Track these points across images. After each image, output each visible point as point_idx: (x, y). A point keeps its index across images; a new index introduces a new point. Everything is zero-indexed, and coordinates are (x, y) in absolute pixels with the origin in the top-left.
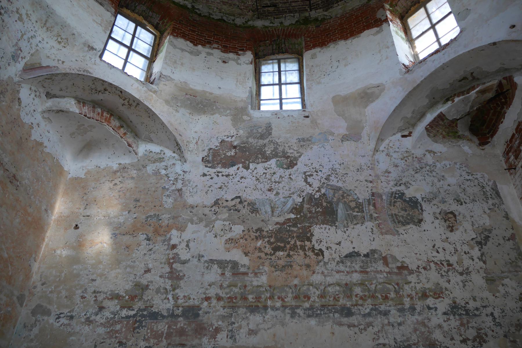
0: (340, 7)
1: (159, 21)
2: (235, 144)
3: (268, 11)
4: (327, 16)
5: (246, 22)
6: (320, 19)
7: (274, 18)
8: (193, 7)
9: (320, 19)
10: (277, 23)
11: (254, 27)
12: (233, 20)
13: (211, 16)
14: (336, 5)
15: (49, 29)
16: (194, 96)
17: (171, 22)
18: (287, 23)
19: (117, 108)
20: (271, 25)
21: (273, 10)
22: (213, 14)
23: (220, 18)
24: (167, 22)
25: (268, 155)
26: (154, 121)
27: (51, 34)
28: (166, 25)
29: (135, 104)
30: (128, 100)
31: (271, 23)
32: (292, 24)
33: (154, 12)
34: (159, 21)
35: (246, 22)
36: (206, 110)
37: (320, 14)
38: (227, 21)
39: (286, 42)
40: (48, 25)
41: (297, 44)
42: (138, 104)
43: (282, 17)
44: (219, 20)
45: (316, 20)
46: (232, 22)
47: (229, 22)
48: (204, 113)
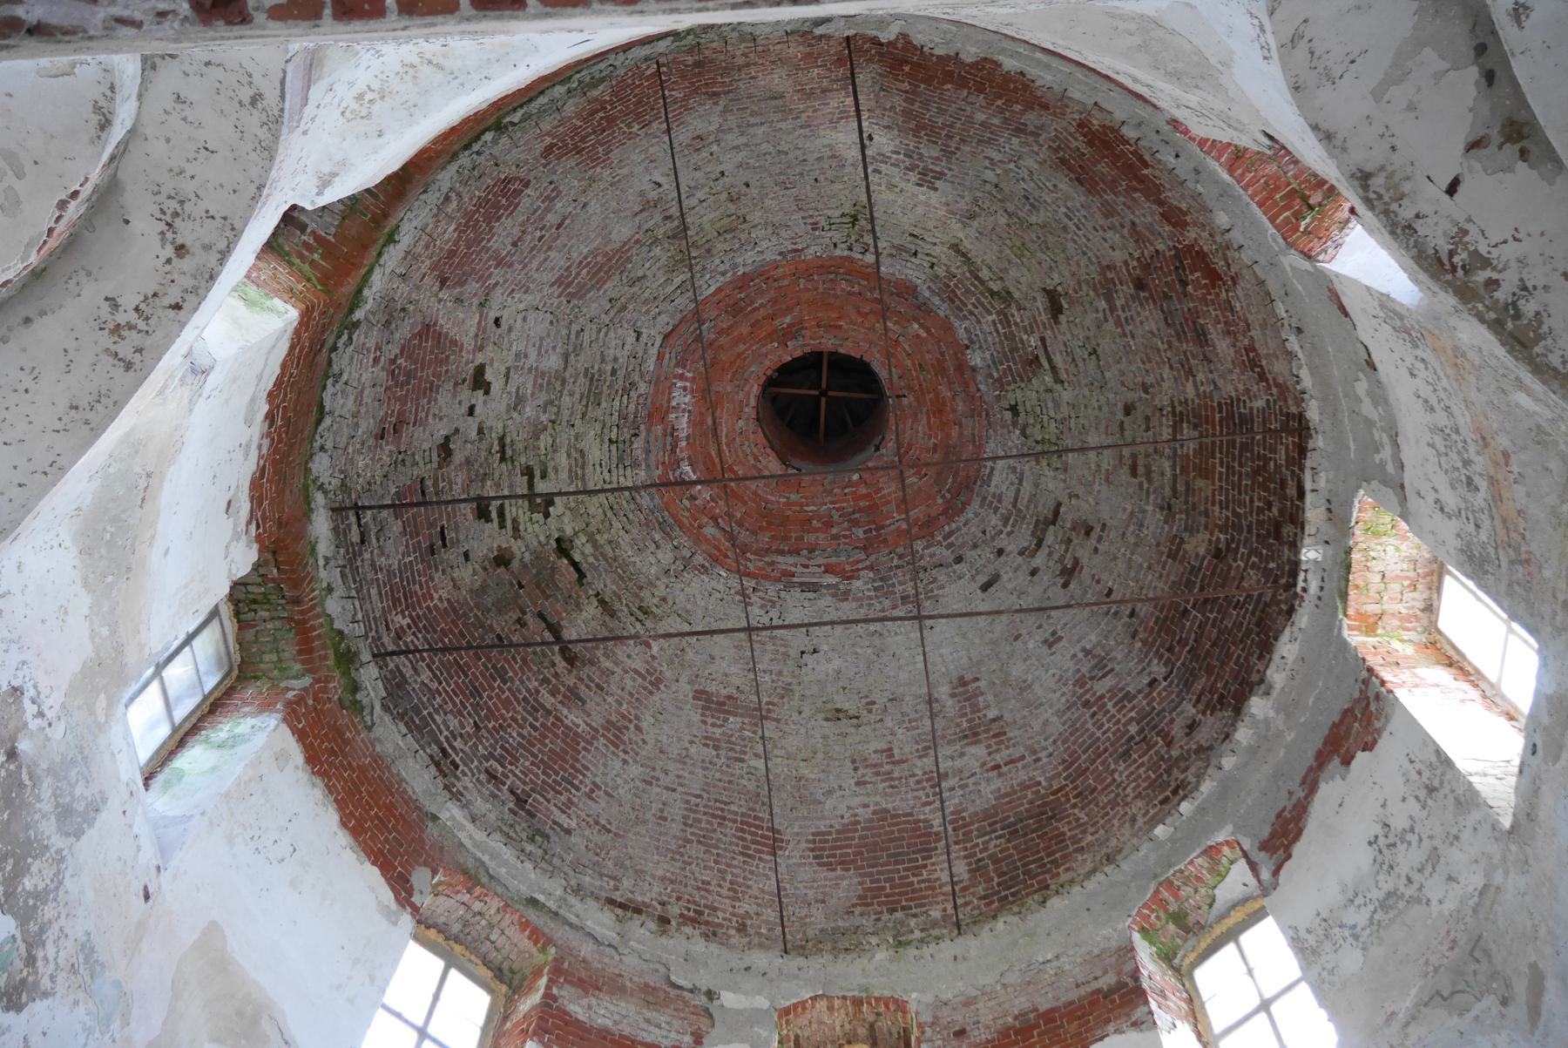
0: (401, 743)
1: (313, 232)
2: (24, 746)
3: (349, 526)
4: (372, 713)
5: (321, 487)
6: (358, 697)
7: (344, 566)
8: (356, 325)
9: (358, 697)
10: (327, 575)
11: (307, 512)
12: (322, 448)
13: (330, 382)
14: (404, 730)
15: (411, 71)
16: (143, 500)
17: (319, 280)
18: (333, 606)
19: (89, 274)
20: (321, 562)
21: (354, 540)
22: (338, 386)
23: (327, 409)
24: (313, 263)
25: (20, 889)
26: (59, 426)
27: (392, 76)
28: (301, 257)
29: (125, 350)
30: (142, 325)
31: (327, 560)
32: (332, 621)
33: (343, 218)
34: (313, 232)
35: (321, 487)
36: (97, 555)
37: (372, 694)
38: (321, 428)
39: (278, 624)
40: (426, 70)
41: (280, 660)
42: (129, 366)
43: (349, 589)
44: (321, 406)
45: (355, 688)
46: (317, 445)
47: (317, 437)
48: (85, 552)
